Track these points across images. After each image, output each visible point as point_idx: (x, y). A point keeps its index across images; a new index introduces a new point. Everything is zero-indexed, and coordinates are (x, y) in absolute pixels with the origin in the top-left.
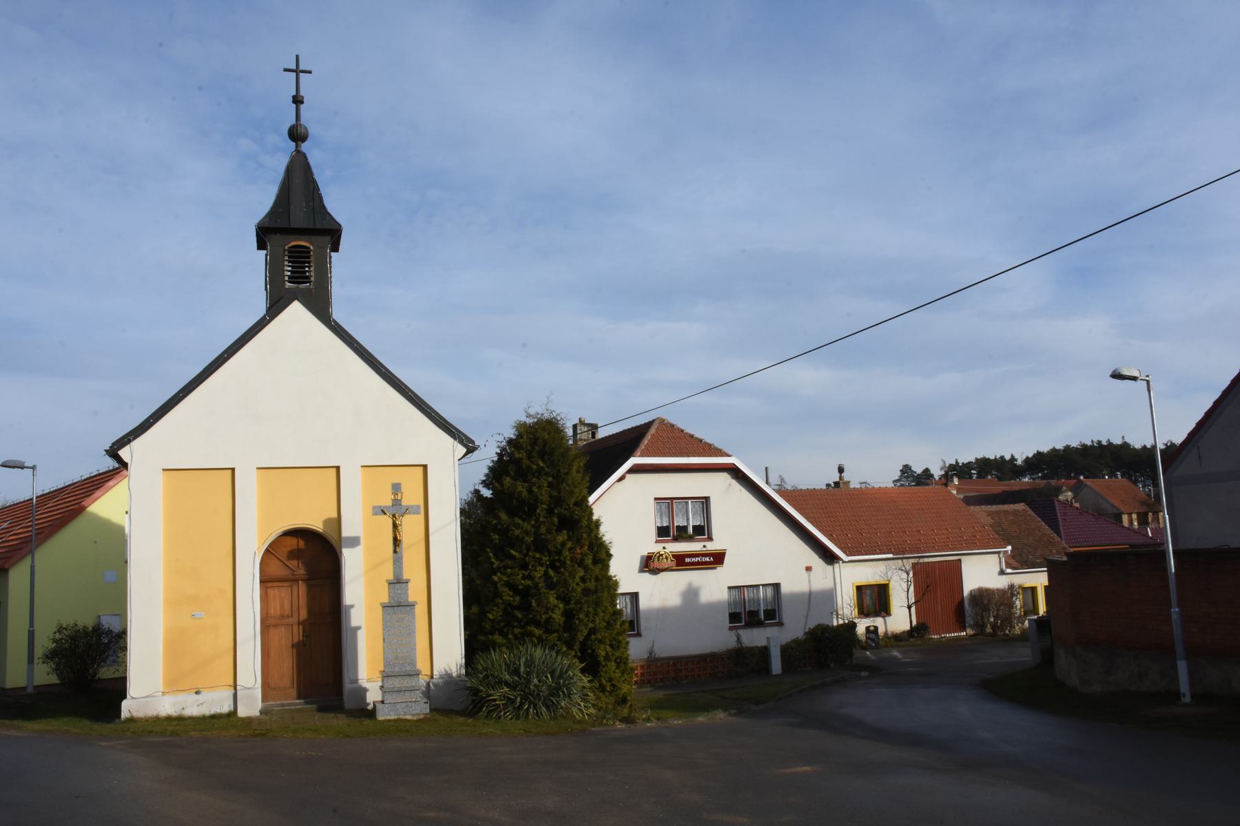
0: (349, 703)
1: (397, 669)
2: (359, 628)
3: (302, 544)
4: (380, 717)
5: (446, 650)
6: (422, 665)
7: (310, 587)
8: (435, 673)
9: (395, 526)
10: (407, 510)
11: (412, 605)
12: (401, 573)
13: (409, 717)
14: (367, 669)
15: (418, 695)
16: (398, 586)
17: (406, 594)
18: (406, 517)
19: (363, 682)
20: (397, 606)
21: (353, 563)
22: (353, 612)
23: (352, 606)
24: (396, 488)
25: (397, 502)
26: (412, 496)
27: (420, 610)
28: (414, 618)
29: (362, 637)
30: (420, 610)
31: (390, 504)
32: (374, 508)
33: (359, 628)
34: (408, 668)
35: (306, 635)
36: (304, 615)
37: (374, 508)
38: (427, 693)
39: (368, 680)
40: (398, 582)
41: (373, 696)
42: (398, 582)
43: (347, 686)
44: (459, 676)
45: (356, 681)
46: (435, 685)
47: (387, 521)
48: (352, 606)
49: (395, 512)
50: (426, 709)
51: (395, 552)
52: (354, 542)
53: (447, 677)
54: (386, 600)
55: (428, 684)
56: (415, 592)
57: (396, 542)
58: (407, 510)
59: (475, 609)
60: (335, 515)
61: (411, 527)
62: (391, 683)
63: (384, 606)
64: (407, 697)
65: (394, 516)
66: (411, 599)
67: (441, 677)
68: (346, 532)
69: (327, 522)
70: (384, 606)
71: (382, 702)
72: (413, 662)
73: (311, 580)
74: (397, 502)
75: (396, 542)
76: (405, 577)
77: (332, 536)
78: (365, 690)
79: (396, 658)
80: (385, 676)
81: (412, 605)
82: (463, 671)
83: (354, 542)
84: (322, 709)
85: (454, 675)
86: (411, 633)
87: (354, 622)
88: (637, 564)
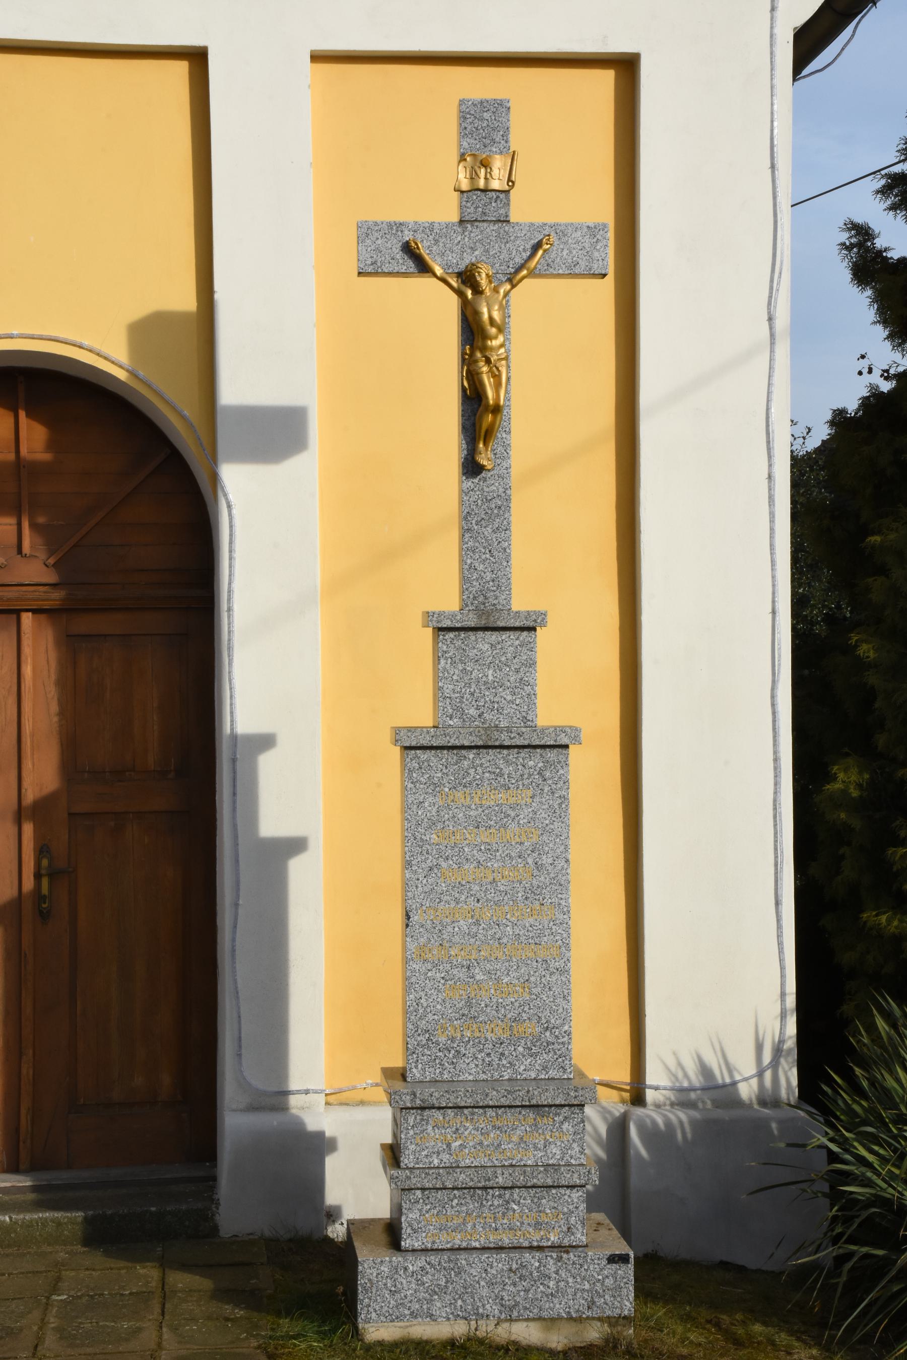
0: (238, 1210)
1: (469, 1071)
2: (296, 846)
3: (35, 439)
4: (378, 1329)
5: (714, 979)
6: (597, 1053)
7: (72, 645)
8: (655, 1075)
9: (473, 332)
10: (537, 255)
11: (557, 746)
12: (501, 584)
13: (527, 1333)
14: (329, 1042)
15: (568, 1214)
16: (483, 643)
17: (524, 687)
18: (528, 287)
19: (315, 1114)
20: (476, 746)
21: (266, 527)
22: (267, 763)
23: (266, 742)
24: (483, 130)
25: (483, 205)
26: (556, 174)
27: (591, 769)
28: (561, 808)
29: (308, 889)
30: (591, 769)
31: (447, 211)
32: (366, 231)
33: (297, 845)
34: (528, 1068)
35: (54, 868)
36: (43, 775)
37: (366, 231)
38: (616, 1192)
39: (336, 1099)
40: (484, 624)
41: (355, 1189)
42: (484, 624)
43: (235, 1123)
44: (769, 1100)
45: (276, 1099)
46: (651, 1135)
47: (434, 307)
48: (266, 742)
49: (466, 262)
50: (619, 1292)
51: (472, 467)
52: (278, 433)
53: (712, 1098)
54: (420, 713)
55: (619, 1128)
56: (568, 684)
57: (479, 415)
58: (537, 255)
59: (847, 778)
60: (185, 300)
61: (551, 335)
62: (429, 1144)
63: (412, 747)
64: (521, 1219)
65: (468, 277)
66: (549, 714)
67: (683, 1098)
68: (236, 387)
69: (147, 331)
70: (412, 747)
71: (392, 1233)
72: (553, 1039)
73: (79, 607)
74: (483, 205)
75: (479, 415)
76: (521, 600)
77: (170, 402)
78: (319, 1146)
79: (469, 1012)
80: (412, 1097)
81: (557, 746)
82: (789, 1076)
83: (278, 433)
84: (104, 1235)
85: (747, 1091)
86: (546, 887)
87: (274, 819)
88: (281, 740)
